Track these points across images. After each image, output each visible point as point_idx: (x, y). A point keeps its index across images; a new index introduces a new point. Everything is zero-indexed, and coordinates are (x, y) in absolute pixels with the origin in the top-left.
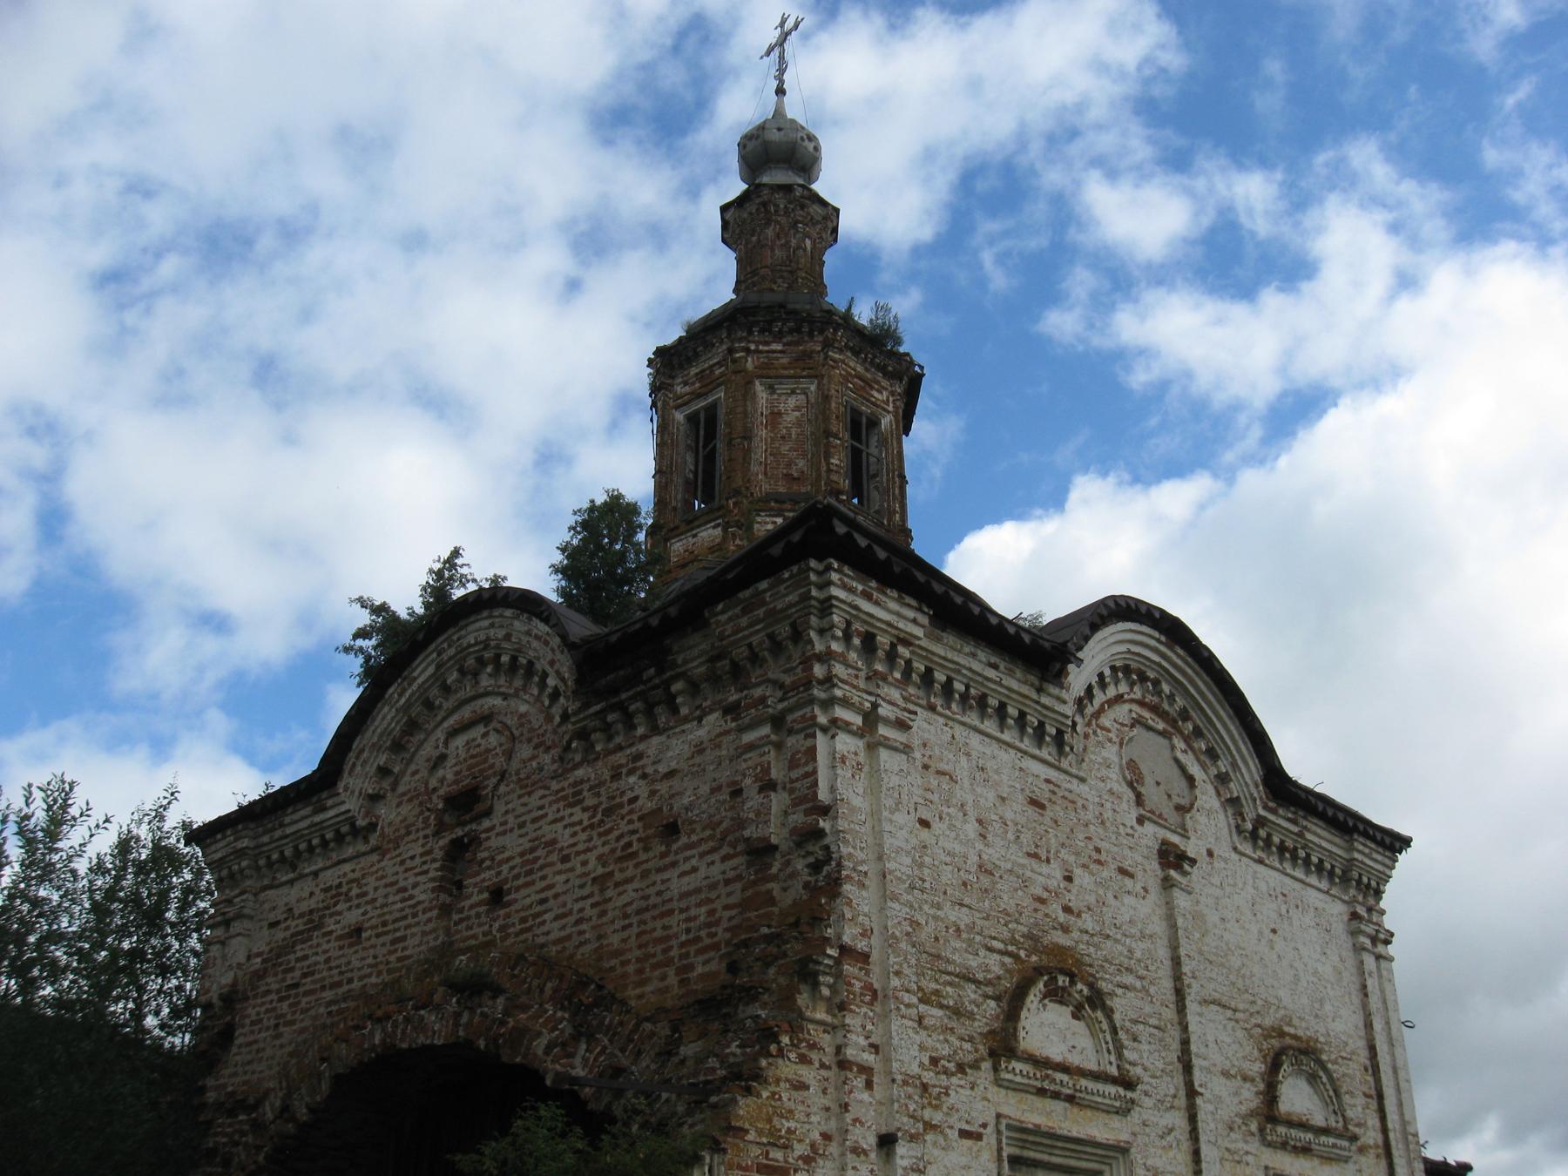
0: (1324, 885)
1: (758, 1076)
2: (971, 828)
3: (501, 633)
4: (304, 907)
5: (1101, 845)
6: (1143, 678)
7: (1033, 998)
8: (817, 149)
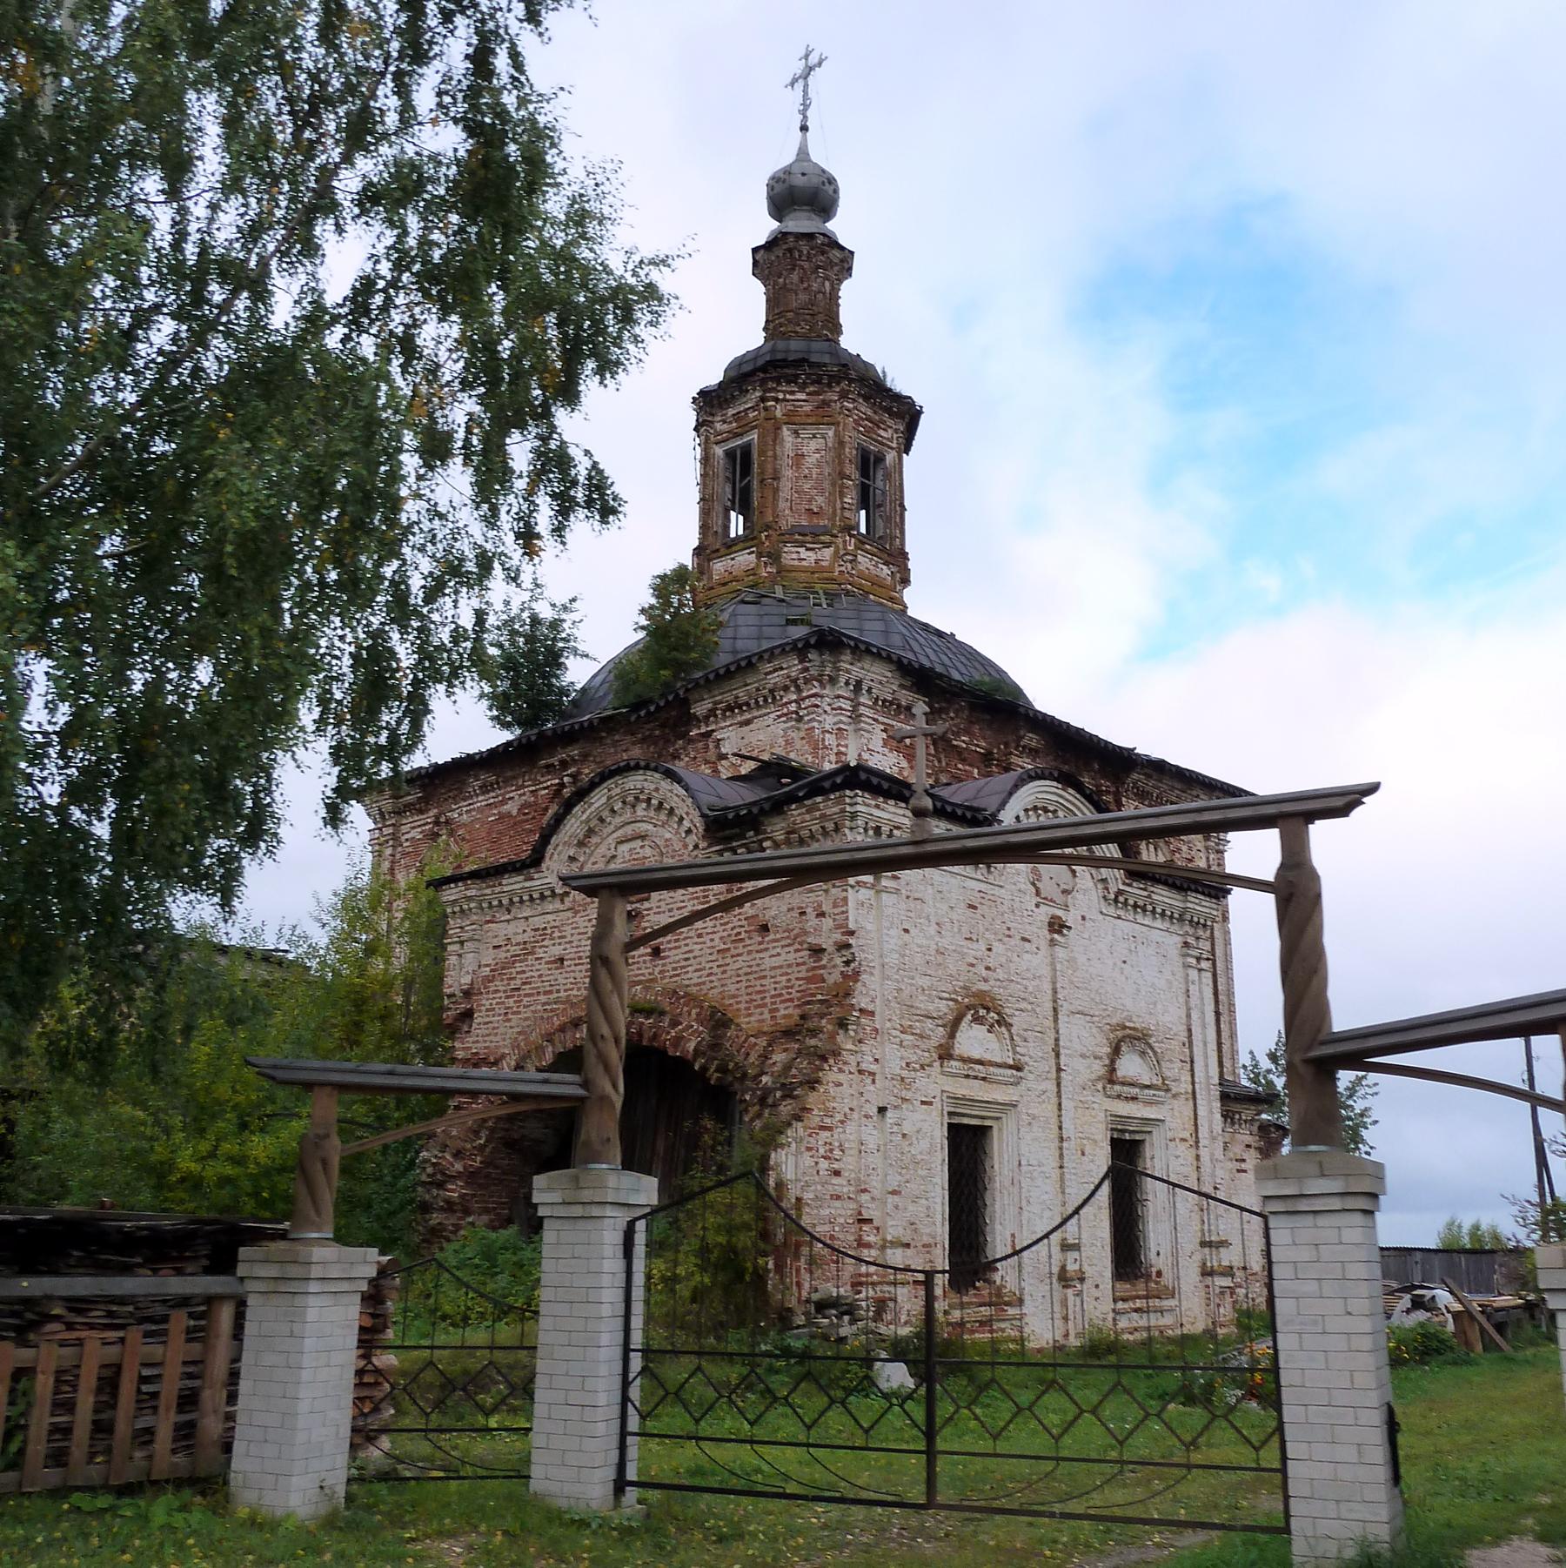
0: (1167, 924)
1: (818, 1081)
2: (933, 929)
3: (653, 787)
4: (520, 938)
5: (1010, 925)
6: (1046, 810)
7: (964, 1025)
8: (836, 191)
